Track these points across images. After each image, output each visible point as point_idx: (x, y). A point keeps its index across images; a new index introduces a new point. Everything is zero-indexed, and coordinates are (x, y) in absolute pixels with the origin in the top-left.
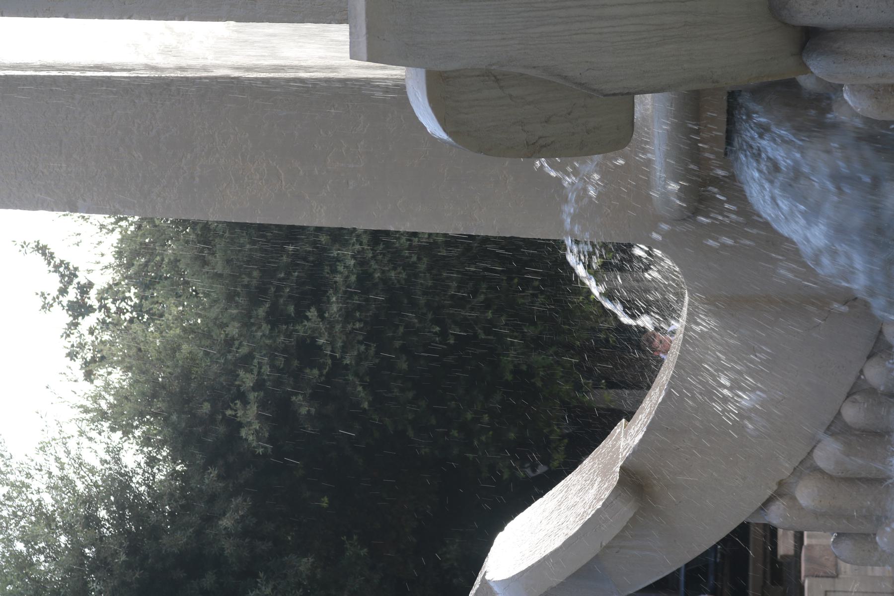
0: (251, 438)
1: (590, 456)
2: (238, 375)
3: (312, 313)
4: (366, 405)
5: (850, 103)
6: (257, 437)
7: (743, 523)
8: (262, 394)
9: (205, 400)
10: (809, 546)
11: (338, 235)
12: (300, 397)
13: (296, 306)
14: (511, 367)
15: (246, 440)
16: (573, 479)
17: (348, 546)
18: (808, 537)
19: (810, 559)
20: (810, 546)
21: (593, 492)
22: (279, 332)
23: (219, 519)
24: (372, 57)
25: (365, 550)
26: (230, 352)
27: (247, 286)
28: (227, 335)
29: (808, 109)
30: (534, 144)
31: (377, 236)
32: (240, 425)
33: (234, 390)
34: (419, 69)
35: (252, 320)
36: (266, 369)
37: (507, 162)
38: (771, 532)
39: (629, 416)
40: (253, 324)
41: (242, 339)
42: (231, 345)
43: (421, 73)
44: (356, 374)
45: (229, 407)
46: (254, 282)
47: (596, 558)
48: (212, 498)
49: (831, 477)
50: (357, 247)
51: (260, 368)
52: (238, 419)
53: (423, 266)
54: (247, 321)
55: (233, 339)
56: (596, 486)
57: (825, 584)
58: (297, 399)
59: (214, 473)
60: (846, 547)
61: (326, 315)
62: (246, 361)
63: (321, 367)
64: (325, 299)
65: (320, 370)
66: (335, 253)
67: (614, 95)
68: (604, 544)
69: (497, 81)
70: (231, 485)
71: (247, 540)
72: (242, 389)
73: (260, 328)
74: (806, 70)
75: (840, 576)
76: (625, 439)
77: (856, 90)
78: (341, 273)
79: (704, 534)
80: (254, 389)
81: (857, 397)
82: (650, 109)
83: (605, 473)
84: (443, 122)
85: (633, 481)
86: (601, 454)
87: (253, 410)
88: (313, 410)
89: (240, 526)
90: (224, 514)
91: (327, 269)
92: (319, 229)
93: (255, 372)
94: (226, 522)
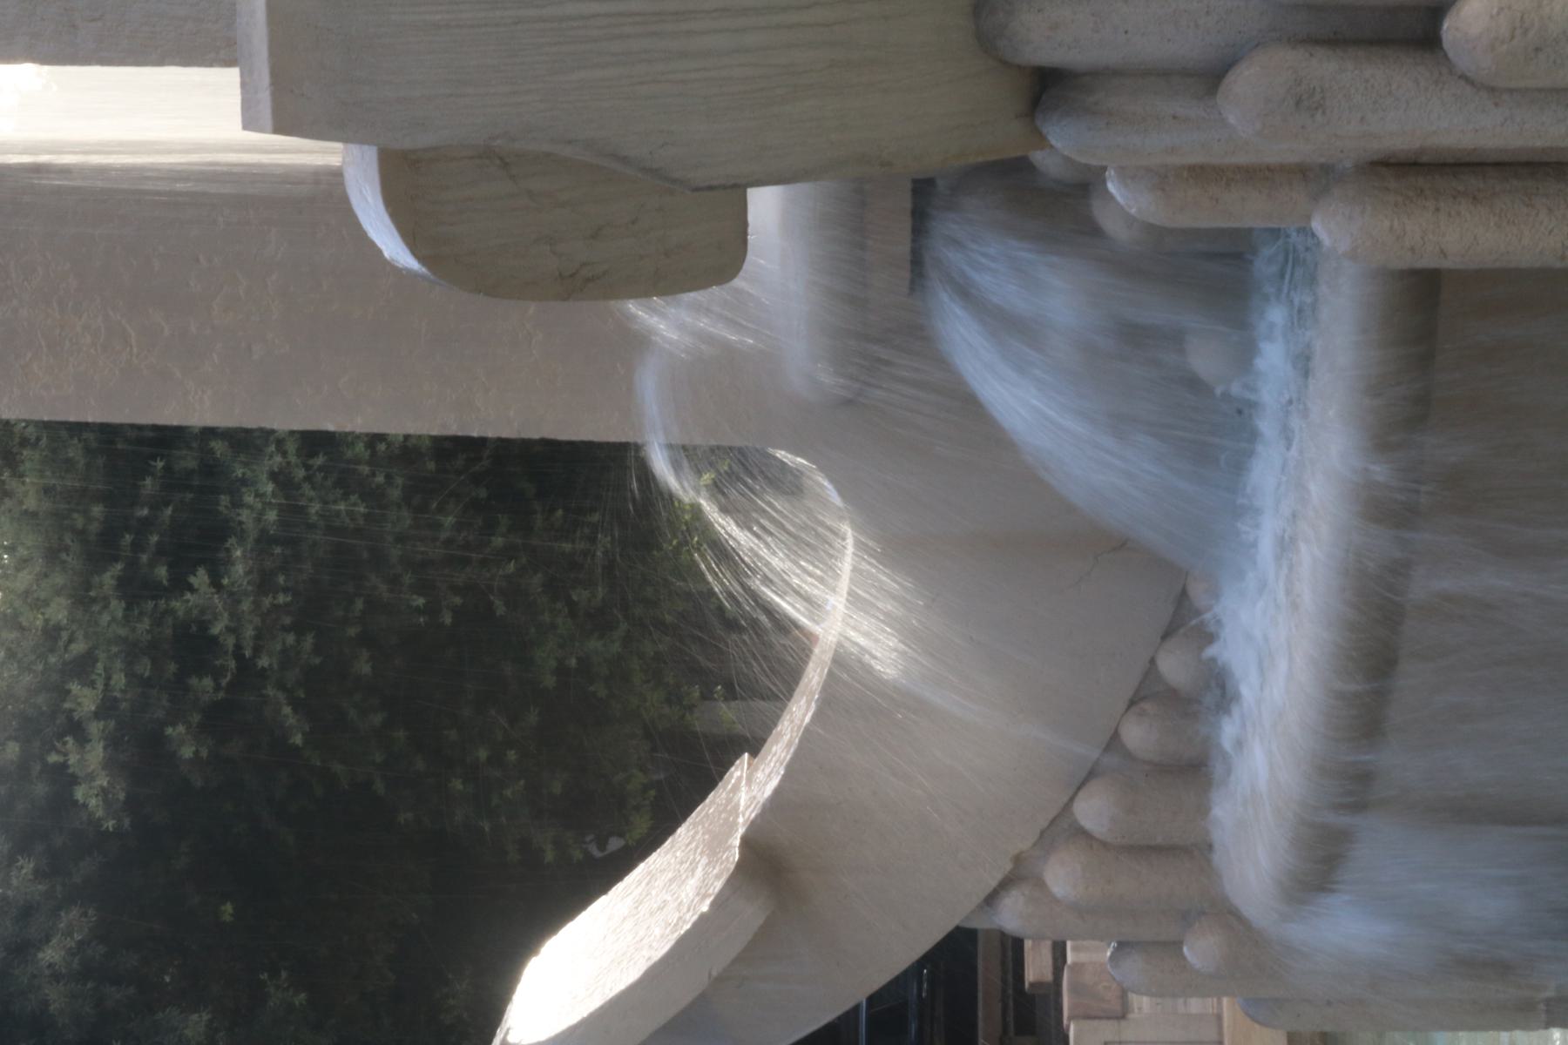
0: (93, 802)
1: (690, 820)
2: (69, 692)
3: (200, 578)
4: (298, 739)
5: (1119, 198)
6: (105, 801)
7: (958, 929)
8: (112, 724)
9: (9, 738)
10: (1075, 964)
11: (245, 441)
12: (181, 729)
13: (171, 566)
14: (553, 663)
15: (85, 806)
16: (656, 861)
17: (272, 990)
18: (1075, 949)
19: (1076, 989)
20: (1078, 967)
21: (693, 883)
22: (141, 613)
23: (39, 949)
24: (283, 125)
25: (303, 996)
26: (52, 651)
27: (83, 532)
28: (47, 621)
29: (1055, 208)
30: (572, 276)
31: (315, 442)
32: (74, 780)
33: (61, 719)
34: (366, 147)
35: (92, 594)
36: (119, 680)
37: (532, 308)
38: (1013, 948)
39: (755, 746)
40: (94, 600)
41: (74, 627)
42: (56, 639)
43: (370, 154)
44: (281, 686)
45: (53, 748)
46: (94, 527)
47: (702, 1000)
48: (27, 912)
49: (1105, 845)
50: (278, 459)
51: (108, 678)
52: (71, 770)
53: (395, 494)
54: (83, 598)
55: (58, 628)
56: (699, 872)
57: (1107, 1030)
58: (175, 731)
59: (27, 866)
60: (1134, 968)
61: (225, 581)
62: (81, 668)
63: (217, 674)
64: (222, 555)
65: (215, 680)
66: (239, 472)
67: (711, 188)
68: (714, 973)
69: (505, 165)
70: (59, 888)
71: (90, 985)
72: (76, 716)
73: (106, 607)
74: (1041, 141)
75: (1130, 1016)
76: (748, 788)
77: (1125, 175)
78: (250, 507)
79: (889, 947)
80: (97, 715)
81: (1147, 706)
82: (766, 207)
83: (714, 847)
84: (412, 239)
85: (764, 863)
86: (707, 815)
87: (96, 753)
88: (204, 753)
89: (76, 960)
90: (47, 939)
91: (224, 500)
92: (209, 433)
93: (100, 686)
94: (51, 955)
